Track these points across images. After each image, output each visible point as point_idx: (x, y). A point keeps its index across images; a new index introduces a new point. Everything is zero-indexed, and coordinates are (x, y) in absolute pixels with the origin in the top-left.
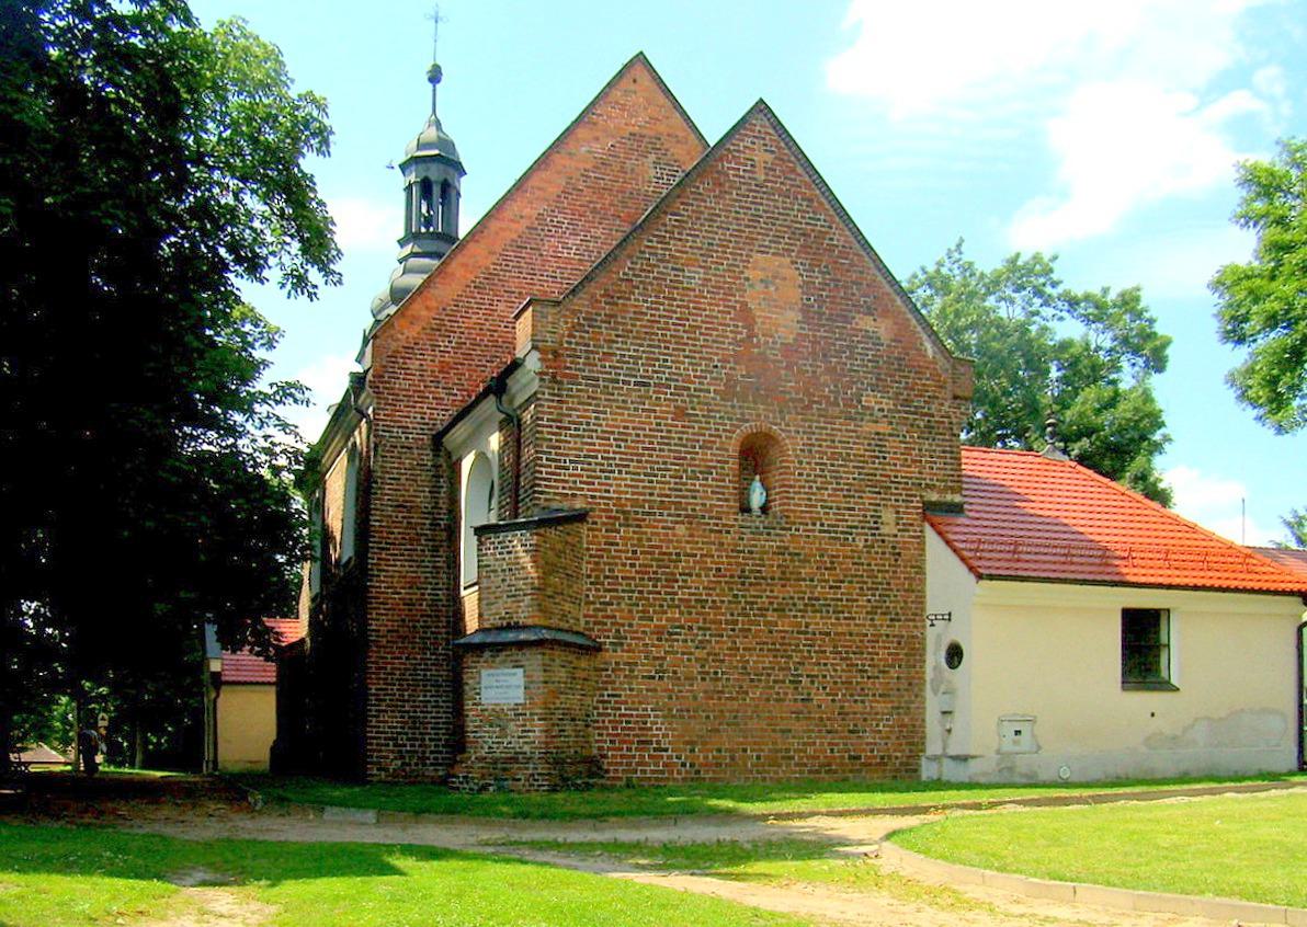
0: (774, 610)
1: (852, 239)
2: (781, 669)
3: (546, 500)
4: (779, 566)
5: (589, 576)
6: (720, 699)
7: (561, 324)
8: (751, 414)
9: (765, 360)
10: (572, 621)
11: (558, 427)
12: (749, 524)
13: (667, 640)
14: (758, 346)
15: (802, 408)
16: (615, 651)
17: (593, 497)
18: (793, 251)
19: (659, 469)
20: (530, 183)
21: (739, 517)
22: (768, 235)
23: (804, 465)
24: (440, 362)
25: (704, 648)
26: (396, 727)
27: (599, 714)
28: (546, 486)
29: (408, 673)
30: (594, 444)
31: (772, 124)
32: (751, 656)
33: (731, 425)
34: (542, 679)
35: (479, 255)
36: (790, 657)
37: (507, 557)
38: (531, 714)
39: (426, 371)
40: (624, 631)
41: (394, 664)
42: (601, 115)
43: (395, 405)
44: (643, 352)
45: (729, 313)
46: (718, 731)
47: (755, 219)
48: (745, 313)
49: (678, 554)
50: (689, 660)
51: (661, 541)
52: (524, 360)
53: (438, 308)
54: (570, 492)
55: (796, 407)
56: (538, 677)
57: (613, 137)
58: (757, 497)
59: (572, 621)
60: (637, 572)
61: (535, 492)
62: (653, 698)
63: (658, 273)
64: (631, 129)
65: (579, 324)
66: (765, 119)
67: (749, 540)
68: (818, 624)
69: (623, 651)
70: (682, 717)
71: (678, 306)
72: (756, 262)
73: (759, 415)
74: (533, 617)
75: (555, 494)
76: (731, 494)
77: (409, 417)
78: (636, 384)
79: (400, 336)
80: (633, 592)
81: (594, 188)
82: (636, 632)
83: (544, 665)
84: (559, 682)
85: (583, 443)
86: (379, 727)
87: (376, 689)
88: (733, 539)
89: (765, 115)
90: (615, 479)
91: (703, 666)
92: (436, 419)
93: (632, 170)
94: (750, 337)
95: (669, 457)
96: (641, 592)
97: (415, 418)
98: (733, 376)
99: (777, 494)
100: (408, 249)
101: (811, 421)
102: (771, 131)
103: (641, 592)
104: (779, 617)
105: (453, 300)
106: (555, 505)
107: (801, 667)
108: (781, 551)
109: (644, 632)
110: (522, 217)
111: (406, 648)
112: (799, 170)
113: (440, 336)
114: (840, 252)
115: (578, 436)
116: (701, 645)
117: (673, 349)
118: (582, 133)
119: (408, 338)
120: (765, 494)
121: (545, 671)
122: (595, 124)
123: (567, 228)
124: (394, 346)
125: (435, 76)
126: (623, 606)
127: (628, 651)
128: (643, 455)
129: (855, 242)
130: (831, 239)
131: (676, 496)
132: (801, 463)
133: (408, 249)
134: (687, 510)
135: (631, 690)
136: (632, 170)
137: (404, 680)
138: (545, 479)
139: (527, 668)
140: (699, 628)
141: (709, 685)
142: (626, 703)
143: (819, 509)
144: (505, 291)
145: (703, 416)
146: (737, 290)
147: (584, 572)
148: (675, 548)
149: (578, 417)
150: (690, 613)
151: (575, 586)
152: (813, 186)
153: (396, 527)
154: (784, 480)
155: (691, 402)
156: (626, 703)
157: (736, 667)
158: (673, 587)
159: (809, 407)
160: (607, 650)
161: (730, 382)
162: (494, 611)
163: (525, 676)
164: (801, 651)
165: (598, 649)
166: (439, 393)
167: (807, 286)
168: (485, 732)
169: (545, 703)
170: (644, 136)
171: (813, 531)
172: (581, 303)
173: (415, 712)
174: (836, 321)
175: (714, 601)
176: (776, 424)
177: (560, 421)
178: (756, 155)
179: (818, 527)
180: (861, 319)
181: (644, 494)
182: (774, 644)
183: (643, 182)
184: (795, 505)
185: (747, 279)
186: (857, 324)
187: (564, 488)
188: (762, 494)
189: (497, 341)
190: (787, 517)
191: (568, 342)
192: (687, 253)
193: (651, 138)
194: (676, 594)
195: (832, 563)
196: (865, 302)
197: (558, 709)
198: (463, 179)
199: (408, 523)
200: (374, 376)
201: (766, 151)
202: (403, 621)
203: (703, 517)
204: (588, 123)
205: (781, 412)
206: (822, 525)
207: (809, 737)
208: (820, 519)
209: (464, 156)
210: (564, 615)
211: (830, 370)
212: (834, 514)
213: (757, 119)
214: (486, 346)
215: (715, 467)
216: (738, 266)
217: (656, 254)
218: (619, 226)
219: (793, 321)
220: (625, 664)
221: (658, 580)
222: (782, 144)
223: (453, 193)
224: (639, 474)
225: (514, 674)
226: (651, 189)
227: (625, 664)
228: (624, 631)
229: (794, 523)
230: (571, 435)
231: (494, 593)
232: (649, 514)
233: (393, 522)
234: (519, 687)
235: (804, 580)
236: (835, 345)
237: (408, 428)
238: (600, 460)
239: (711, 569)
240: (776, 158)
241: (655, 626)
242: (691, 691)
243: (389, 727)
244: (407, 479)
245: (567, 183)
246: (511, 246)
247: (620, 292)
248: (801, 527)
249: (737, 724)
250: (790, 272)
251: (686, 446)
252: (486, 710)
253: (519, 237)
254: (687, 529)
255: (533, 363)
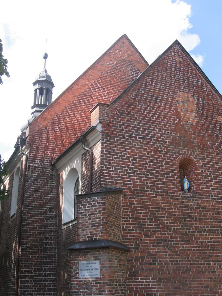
0: (198, 232)
1: (211, 89)
2: (203, 258)
3: (105, 184)
4: (198, 213)
5: (123, 218)
6: (179, 273)
7: (110, 113)
8: (182, 152)
9: (186, 131)
10: (118, 238)
11: (109, 154)
12: (185, 196)
13: (156, 246)
14: (182, 125)
15: (201, 150)
16: (135, 252)
17: (124, 184)
18: (192, 92)
19: (149, 172)
20: (88, 73)
21: (181, 193)
22: (183, 86)
23: (203, 172)
24: (55, 135)
25: (171, 250)
26: (32, 288)
27: (129, 282)
28: (105, 179)
29: (38, 263)
30: (124, 162)
31: (180, 48)
32: (190, 253)
33: (175, 155)
34: (108, 265)
35: (58, 110)
36: (206, 253)
37: (91, 208)
38: (103, 283)
39: (49, 138)
40: (139, 242)
41: (32, 259)
42: (112, 53)
43: (37, 151)
44: (141, 126)
45: (172, 113)
46: (179, 288)
47: (178, 80)
48: (177, 113)
49: (159, 208)
50: (166, 255)
51: (152, 202)
52: (96, 127)
53: (55, 115)
54: (115, 181)
55: (198, 149)
56: (107, 264)
57: (117, 60)
58: (186, 185)
59: (118, 238)
60: (143, 216)
61: (101, 181)
62: (152, 273)
63: (145, 97)
64: (122, 58)
65: (117, 114)
66: (178, 47)
67: (186, 202)
68: (215, 238)
69: (138, 252)
70: (164, 282)
71: (153, 109)
72: (179, 95)
73: (185, 152)
74: (104, 236)
75: (109, 182)
76: (177, 183)
77: (42, 156)
78: (139, 138)
79: (40, 125)
80: (142, 225)
81: (111, 76)
82: (144, 243)
83: (109, 258)
84: (115, 267)
85: (119, 161)
86: (25, 288)
87: (25, 271)
88: (179, 202)
89: (178, 45)
90: (132, 176)
91: (171, 258)
92: (53, 157)
93: (123, 71)
94: (180, 122)
95: (153, 167)
96: (145, 225)
97: (44, 156)
98: (175, 136)
99: (194, 183)
100: (34, 110)
101: (204, 154)
102: (181, 51)
103: (145, 225)
104: (200, 235)
105: (60, 113)
106: (109, 186)
107: (210, 257)
108: (198, 207)
109: (147, 243)
110: (85, 85)
111: (38, 252)
112: (191, 64)
113: (55, 125)
114: (207, 93)
115: (117, 158)
116: (170, 248)
117: (152, 125)
118: (106, 58)
119: (43, 126)
120: (189, 183)
121: (110, 261)
122: (110, 55)
123: (102, 90)
124: (37, 128)
125: (46, 57)
126: (137, 231)
127: (141, 252)
128: (143, 166)
129: (212, 90)
130: (204, 88)
131: (157, 184)
132: (202, 171)
133: (34, 110)
134: (161, 189)
135: (143, 269)
136: (123, 71)
137: (36, 266)
138: (104, 176)
139: (101, 260)
140: (169, 241)
141: (174, 267)
142: (141, 276)
143: (211, 190)
144: (79, 110)
145: (165, 151)
146: (174, 104)
147: (121, 216)
148: (157, 205)
149: (117, 150)
150: (165, 234)
151: (118, 222)
152: (196, 70)
153: (35, 200)
154: (197, 177)
155: (160, 146)
156: (141, 276)
157: (185, 258)
158: (158, 223)
159: (203, 149)
160: (132, 251)
161: (174, 139)
162: (85, 233)
163: (100, 264)
164: (210, 250)
165: (128, 251)
166: (54, 147)
167: (198, 104)
168: (81, 292)
169: (110, 277)
170: (127, 61)
171: (209, 198)
172: (117, 105)
173: (41, 281)
174: (209, 117)
175: (174, 229)
176: (191, 155)
177: (111, 152)
178: (177, 58)
179: (211, 197)
180: (218, 117)
181: (144, 183)
182: (199, 247)
183: (127, 75)
184: (202, 188)
185: (177, 101)
186: (216, 119)
187: (112, 179)
188: (188, 183)
189: (76, 128)
190: (199, 193)
191: (112, 121)
192: (155, 90)
193: (129, 61)
194: (159, 225)
195: (218, 212)
196: (218, 111)
197: (114, 280)
198: (53, 88)
199: (40, 198)
200: (29, 140)
201: (179, 57)
202: (37, 240)
203: (167, 193)
204: (108, 55)
205: (193, 151)
206: (212, 196)
207: (216, 289)
208: (211, 194)
209: (54, 80)
210: (115, 235)
211: (209, 135)
212: (216, 192)
213: (175, 47)
214: (72, 130)
215: (171, 172)
216: (173, 96)
217: (144, 90)
218: (119, 89)
219: (194, 117)
220: (139, 258)
221: (152, 219)
222: (185, 56)
223: (50, 93)
224: (142, 174)
225: (95, 263)
226: (130, 78)
227: (139, 258)
228: (139, 242)
229: (202, 195)
230: (115, 158)
231: (85, 225)
232: (146, 191)
233: (34, 198)
234: (97, 269)
235: (208, 219)
236: (210, 126)
237: (42, 160)
238: (126, 168)
239: (172, 215)
240: (183, 60)
241: (151, 240)
242: (167, 270)
243: (29, 288)
244: (41, 180)
245: (101, 74)
246: (82, 94)
247: (131, 103)
248: (205, 197)
249: (187, 284)
250: (191, 99)
251: (159, 163)
252: (82, 281)
253: (84, 91)
254: (162, 197)
255: (99, 128)
